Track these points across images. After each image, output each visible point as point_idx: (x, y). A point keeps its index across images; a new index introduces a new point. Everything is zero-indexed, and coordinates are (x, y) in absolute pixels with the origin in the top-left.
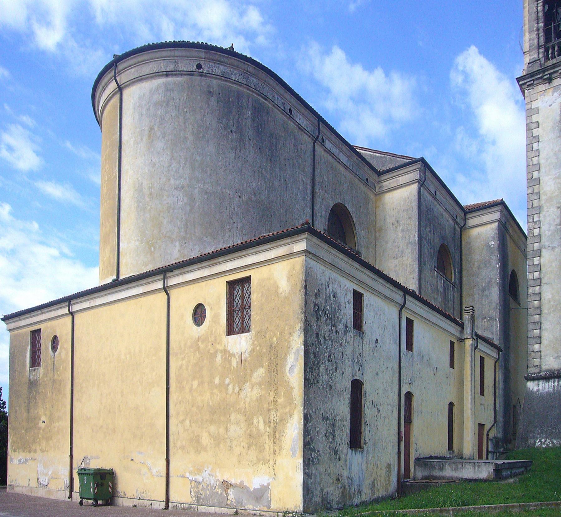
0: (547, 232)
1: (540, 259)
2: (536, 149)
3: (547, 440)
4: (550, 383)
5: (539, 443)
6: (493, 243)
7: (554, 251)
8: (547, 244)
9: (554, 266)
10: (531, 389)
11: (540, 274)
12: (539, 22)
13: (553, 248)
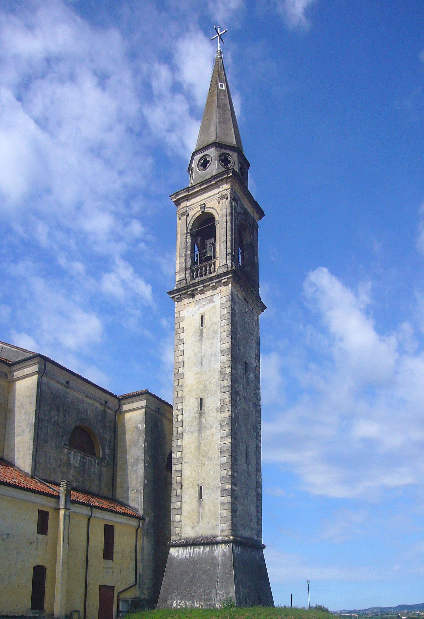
0: (187, 419)
1: (182, 441)
2: (181, 349)
3: (181, 601)
4: (187, 550)
5: (176, 604)
6: (141, 426)
7: (192, 435)
8: (187, 429)
9: (192, 448)
10: (173, 555)
11: (181, 454)
12: (187, 251)
13: (192, 432)
